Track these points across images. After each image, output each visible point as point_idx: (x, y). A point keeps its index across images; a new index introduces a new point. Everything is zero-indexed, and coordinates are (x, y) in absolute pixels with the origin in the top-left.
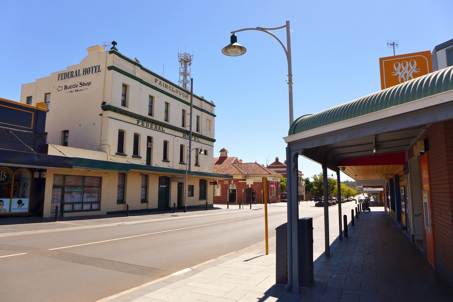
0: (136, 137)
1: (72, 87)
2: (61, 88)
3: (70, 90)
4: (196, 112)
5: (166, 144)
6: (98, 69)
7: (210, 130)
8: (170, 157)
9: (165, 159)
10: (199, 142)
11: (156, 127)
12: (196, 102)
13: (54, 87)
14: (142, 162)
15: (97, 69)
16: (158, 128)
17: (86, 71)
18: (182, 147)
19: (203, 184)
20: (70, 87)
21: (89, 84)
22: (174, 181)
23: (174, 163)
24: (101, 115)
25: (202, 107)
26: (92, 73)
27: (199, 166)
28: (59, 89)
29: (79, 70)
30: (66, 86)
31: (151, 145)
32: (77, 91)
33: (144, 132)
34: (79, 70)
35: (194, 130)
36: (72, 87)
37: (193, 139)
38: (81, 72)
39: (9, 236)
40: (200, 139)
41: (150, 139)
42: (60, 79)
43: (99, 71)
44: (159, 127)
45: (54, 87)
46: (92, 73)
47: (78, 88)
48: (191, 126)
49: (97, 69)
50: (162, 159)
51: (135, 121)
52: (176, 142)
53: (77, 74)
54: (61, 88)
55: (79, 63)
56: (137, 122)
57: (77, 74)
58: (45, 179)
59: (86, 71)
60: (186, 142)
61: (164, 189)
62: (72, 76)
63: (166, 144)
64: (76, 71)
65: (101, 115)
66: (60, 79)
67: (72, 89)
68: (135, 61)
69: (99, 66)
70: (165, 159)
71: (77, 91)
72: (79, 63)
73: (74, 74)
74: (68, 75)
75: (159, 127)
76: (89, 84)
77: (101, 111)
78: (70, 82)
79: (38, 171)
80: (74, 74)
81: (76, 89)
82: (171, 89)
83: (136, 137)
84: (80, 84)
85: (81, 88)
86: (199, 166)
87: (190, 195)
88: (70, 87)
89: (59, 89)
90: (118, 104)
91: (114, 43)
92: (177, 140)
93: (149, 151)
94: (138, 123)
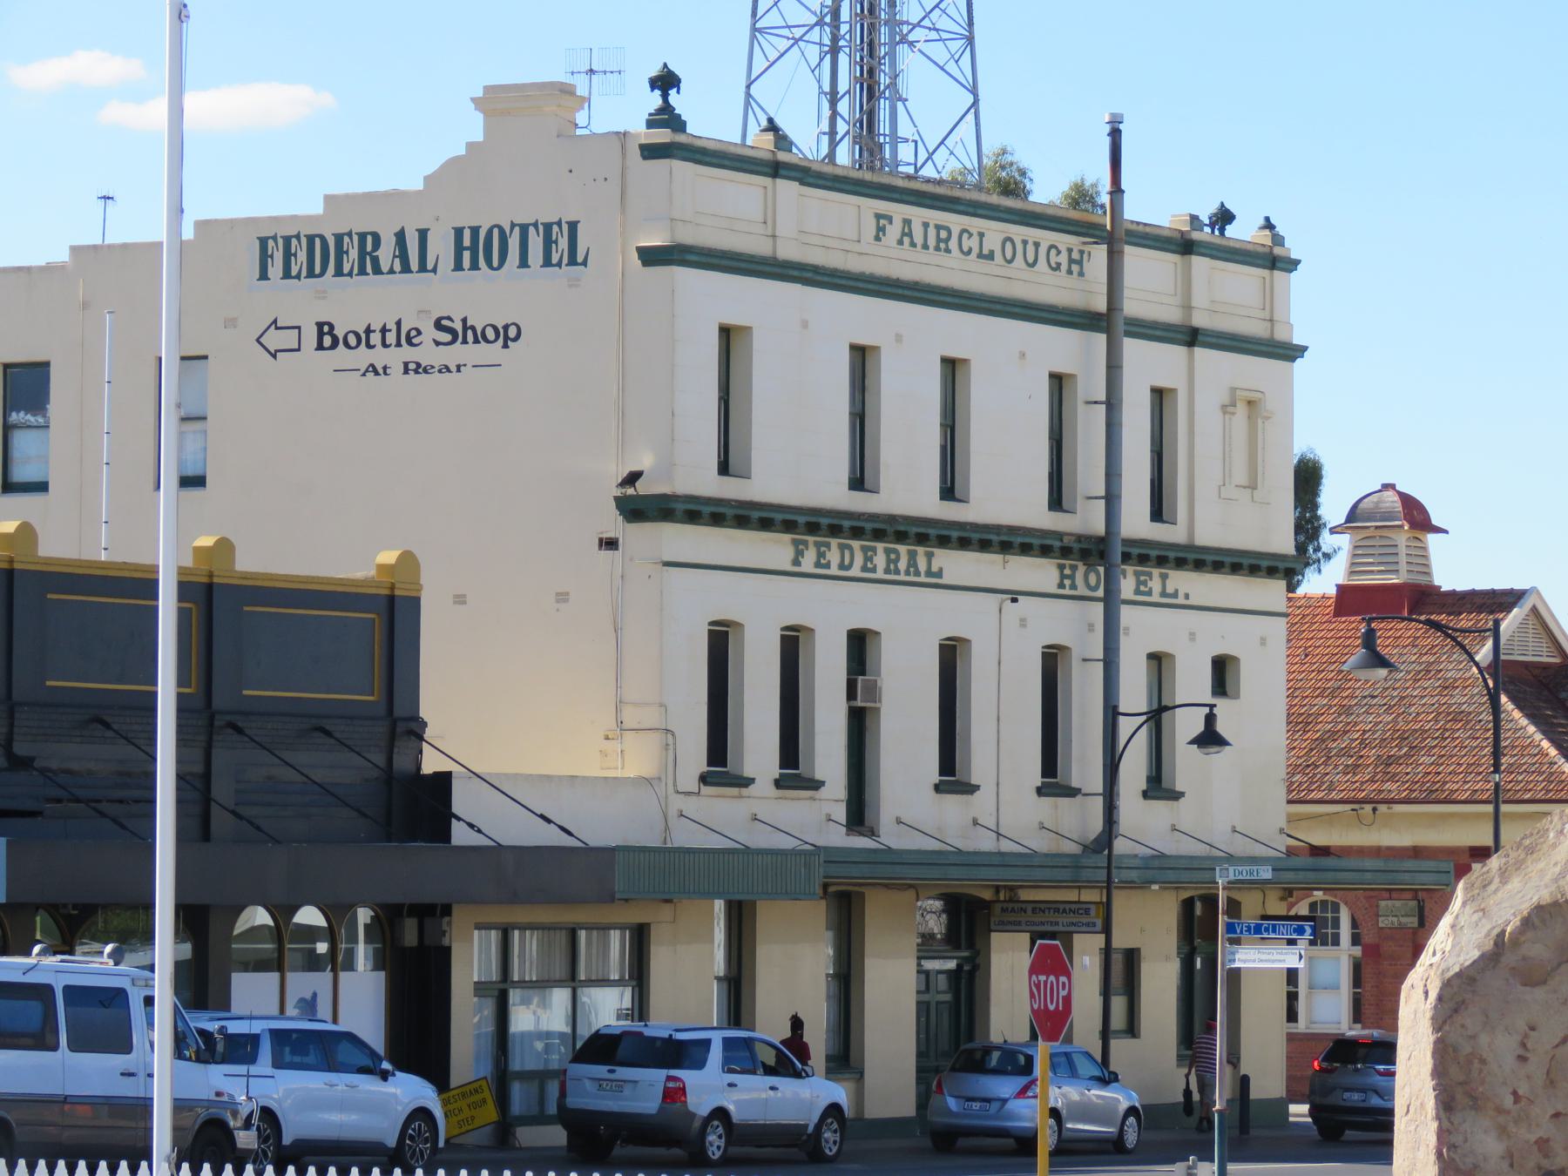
0: (793, 645)
1: (376, 338)
2: (289, 339)
3: (363, 357)
4: (1147, 364)
5: (951, 656)
6: (563, 243)
7: (1252, 486)
8: (980, 762)
9: (951, 772)
10: (1170, 602)
11: (892, 562)
12: (1150, 283)
13: (231, 323)
14: (816, 820)
15: (561, 245)
16: (902, 565)
17: (479, 248)
18: (1053, 662)
19: (1200, 927)
20: (363, 338)
21: (507, 335)
22: (1007, 927)
23: (1008, 810)
24: (610, 544)
25: (1188, 308)
26: (524, 263)
27: (1176, 796)
28: (274, 340)
29: (423, 234)
30: (324, 329)
31: (873, 691)
32: (419, 369)
33: (831, 608)
34: (423, 234)
35: (1136, 522)
36: (376, 338)
37: (1127, 587)
38: (441, 247)
39: (1427, 1063)
40: (1185, 582)
41: (860, 644)
42: (275, 270)
43: (573, 261)
44: (912, 556)
45: (231, 323)
46: (524, 263)
47: (426, 353)
48: (1111, 499)
49: (561, 245)
50: (935, 777)
51: (774, 549)
52: (1014, 622)
53: (411, 255)
54: (289, 339)
55: (418, 185)
56: (789, 553)
57: (411, 255)
58: (448, 950)
59: (479, 248)
60: (1075, 625)
61: (942, 982)
62: (369, 263)
63: (951, 656)
64: (401, 236)
65: (610, 544)
66: (275, 270)
67: (379, 356)
68: (759, 142)
69: (573, 226)
70: (951, 772)
71: (419, 369)
72: (418, 185)
73: (386, 254)
74: (340, 252)
75: (912, 556)
76: (507, 335)
77: (614, 524)
78: (356, 302)
79: (410, 915)
80: (386, 254)
81: (407, 353)
82: (974, 243)
83: (793, 645)
84: (438, 325)
85: (456, 354)
86: (1176, 796)
87: (923, 988)
88: (363, 338)
89: (274, 340)
90: (703, 480)
91: (666, 81)
92: (1023, 622)
93: (860, 724)
94: (796, 562)
